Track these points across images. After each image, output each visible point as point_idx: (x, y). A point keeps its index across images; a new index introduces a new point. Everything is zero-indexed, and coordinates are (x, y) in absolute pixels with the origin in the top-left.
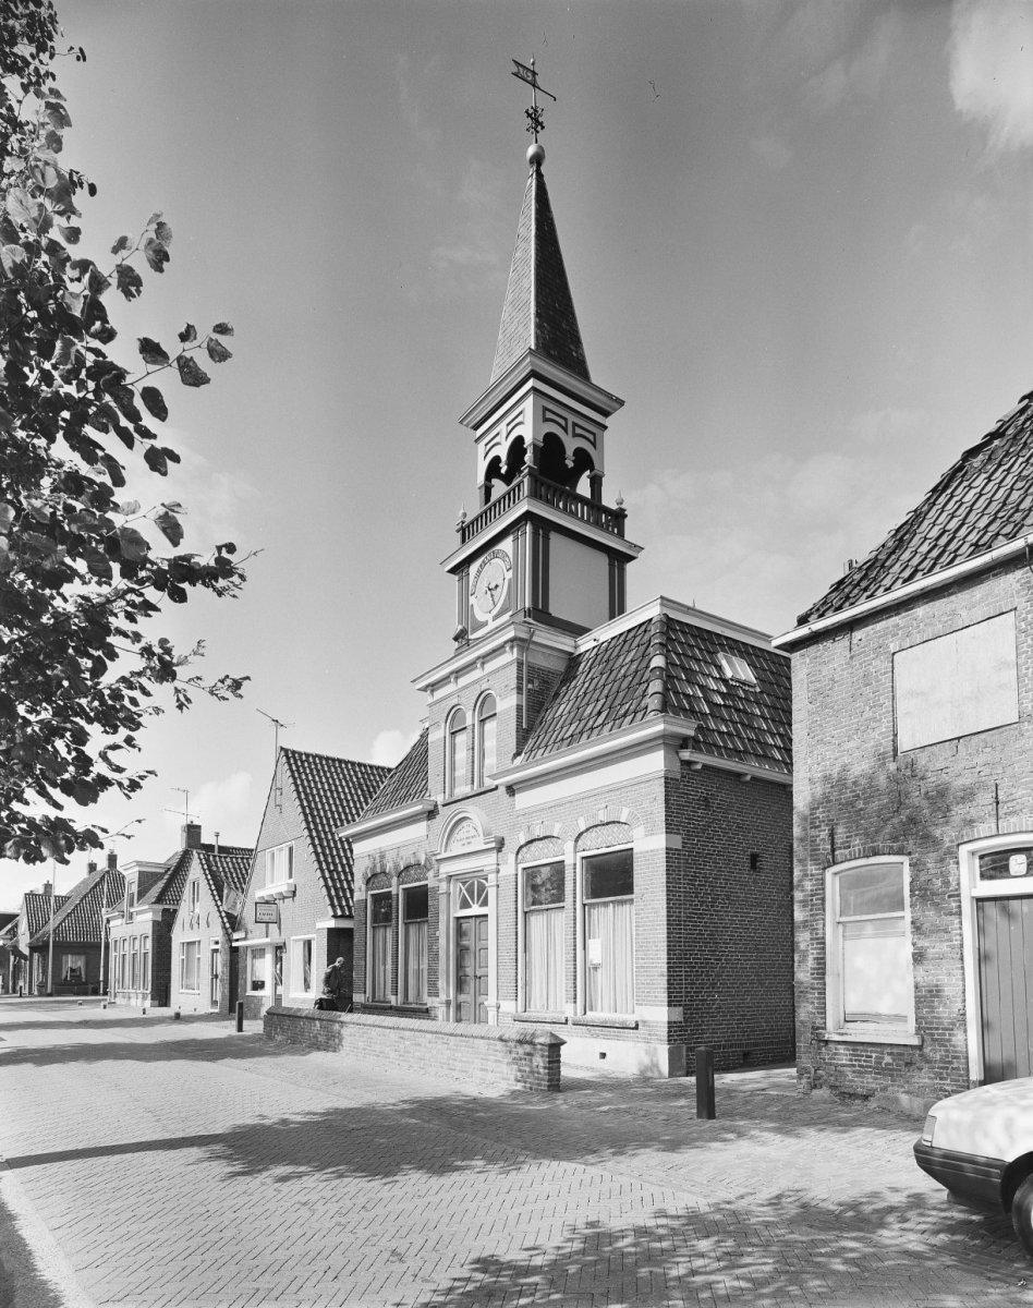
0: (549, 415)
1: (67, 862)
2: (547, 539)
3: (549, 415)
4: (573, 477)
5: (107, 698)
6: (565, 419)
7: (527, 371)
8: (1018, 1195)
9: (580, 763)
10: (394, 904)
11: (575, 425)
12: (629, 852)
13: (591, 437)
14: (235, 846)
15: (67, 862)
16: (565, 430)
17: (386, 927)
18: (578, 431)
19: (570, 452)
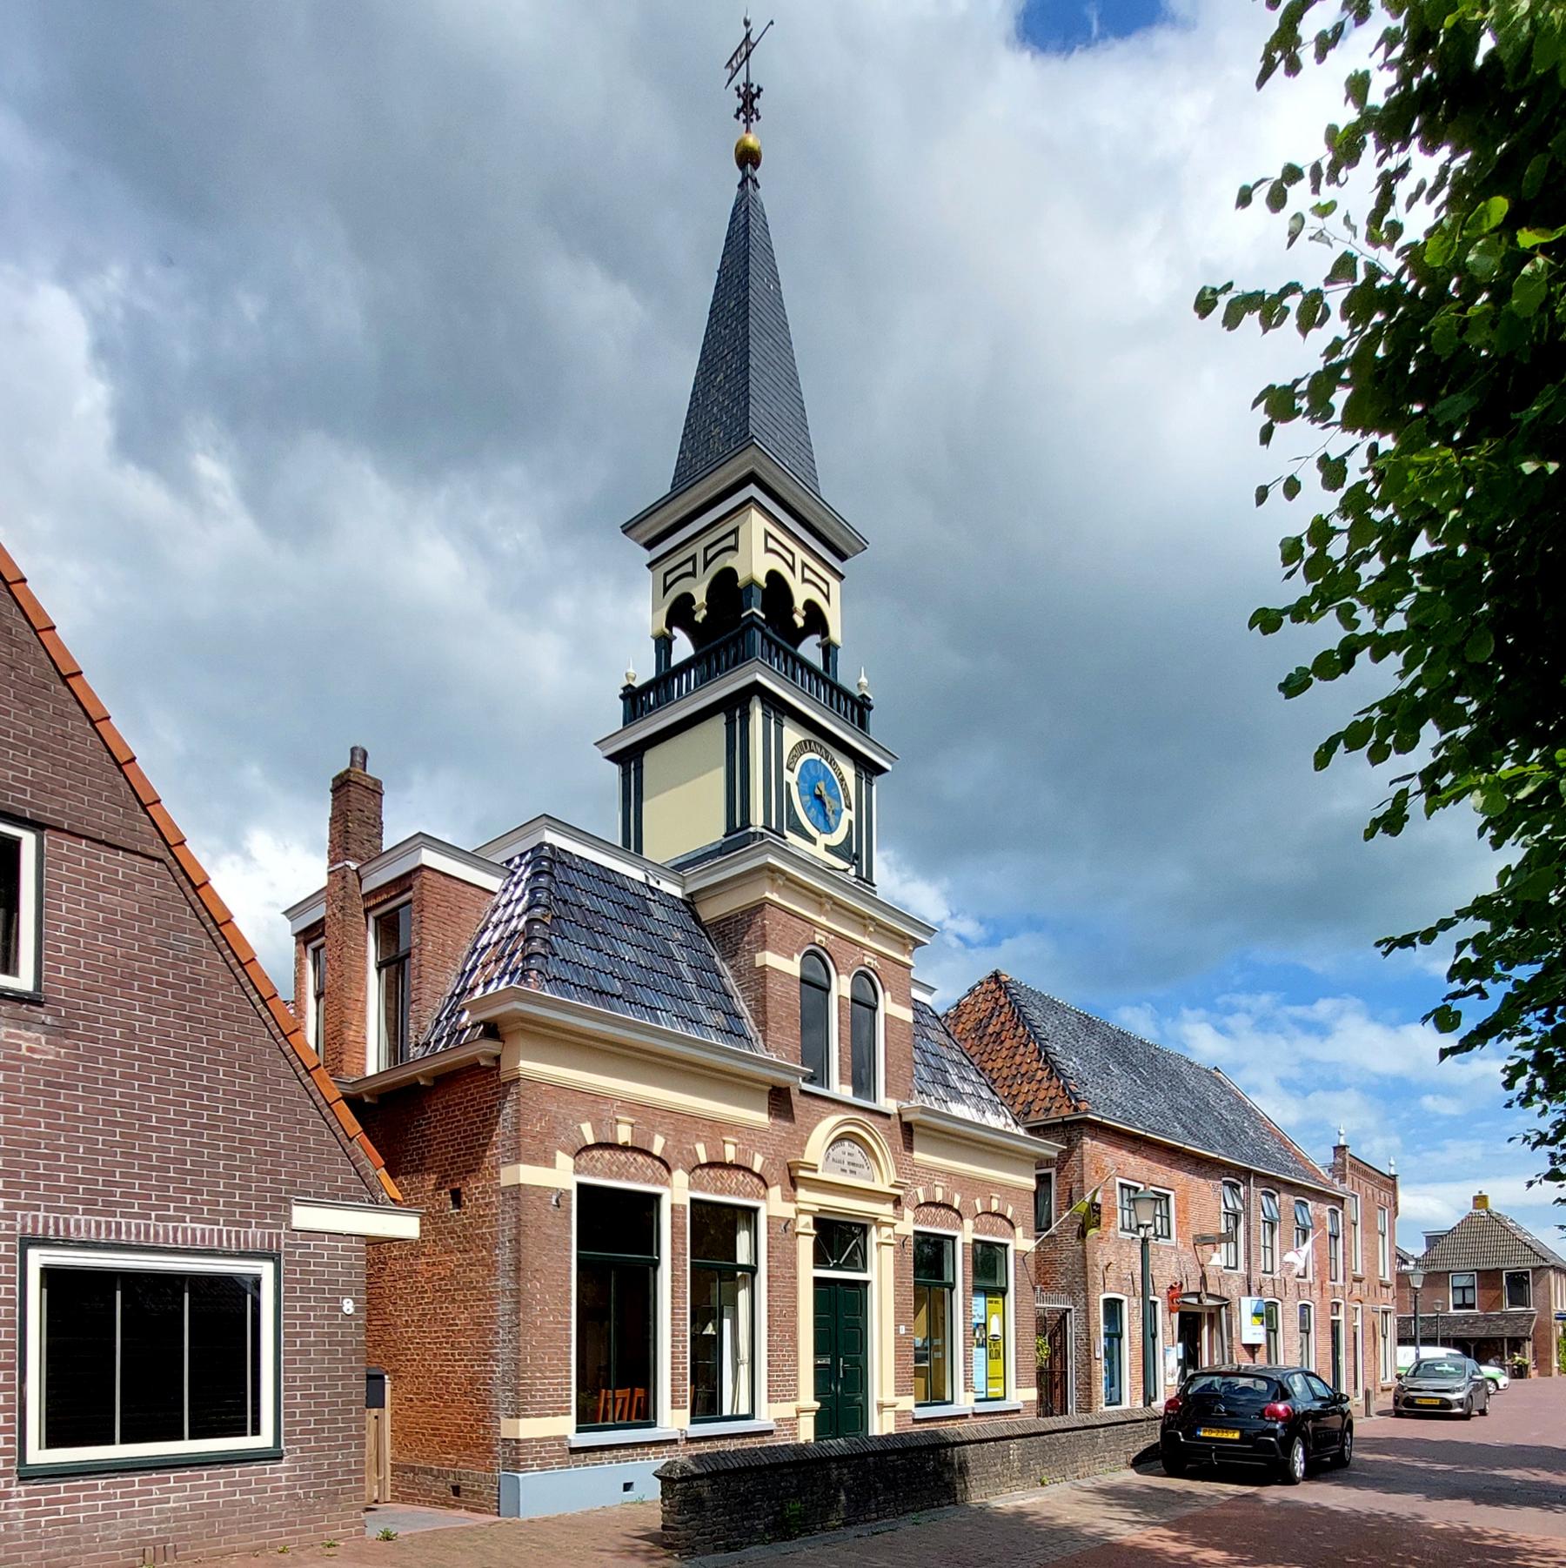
0: (772, 544)
1: (1251, 626)
2: (780, 725)
3: (772, 544)
4: (798, 636)
5: (1452, 733)
6: (792, 554)
7: (745, 471)
8: (1149, 1005)
9: (887, 930)
10: (622, 1023)
11: (804, 565)
12: (860, 1265)
13: (824, 587)
14: (1026, 1390)
15: (1251, 626)
16: (792, 569)
17: (734, 707)
18: (808, 574)
19: (799, 604)
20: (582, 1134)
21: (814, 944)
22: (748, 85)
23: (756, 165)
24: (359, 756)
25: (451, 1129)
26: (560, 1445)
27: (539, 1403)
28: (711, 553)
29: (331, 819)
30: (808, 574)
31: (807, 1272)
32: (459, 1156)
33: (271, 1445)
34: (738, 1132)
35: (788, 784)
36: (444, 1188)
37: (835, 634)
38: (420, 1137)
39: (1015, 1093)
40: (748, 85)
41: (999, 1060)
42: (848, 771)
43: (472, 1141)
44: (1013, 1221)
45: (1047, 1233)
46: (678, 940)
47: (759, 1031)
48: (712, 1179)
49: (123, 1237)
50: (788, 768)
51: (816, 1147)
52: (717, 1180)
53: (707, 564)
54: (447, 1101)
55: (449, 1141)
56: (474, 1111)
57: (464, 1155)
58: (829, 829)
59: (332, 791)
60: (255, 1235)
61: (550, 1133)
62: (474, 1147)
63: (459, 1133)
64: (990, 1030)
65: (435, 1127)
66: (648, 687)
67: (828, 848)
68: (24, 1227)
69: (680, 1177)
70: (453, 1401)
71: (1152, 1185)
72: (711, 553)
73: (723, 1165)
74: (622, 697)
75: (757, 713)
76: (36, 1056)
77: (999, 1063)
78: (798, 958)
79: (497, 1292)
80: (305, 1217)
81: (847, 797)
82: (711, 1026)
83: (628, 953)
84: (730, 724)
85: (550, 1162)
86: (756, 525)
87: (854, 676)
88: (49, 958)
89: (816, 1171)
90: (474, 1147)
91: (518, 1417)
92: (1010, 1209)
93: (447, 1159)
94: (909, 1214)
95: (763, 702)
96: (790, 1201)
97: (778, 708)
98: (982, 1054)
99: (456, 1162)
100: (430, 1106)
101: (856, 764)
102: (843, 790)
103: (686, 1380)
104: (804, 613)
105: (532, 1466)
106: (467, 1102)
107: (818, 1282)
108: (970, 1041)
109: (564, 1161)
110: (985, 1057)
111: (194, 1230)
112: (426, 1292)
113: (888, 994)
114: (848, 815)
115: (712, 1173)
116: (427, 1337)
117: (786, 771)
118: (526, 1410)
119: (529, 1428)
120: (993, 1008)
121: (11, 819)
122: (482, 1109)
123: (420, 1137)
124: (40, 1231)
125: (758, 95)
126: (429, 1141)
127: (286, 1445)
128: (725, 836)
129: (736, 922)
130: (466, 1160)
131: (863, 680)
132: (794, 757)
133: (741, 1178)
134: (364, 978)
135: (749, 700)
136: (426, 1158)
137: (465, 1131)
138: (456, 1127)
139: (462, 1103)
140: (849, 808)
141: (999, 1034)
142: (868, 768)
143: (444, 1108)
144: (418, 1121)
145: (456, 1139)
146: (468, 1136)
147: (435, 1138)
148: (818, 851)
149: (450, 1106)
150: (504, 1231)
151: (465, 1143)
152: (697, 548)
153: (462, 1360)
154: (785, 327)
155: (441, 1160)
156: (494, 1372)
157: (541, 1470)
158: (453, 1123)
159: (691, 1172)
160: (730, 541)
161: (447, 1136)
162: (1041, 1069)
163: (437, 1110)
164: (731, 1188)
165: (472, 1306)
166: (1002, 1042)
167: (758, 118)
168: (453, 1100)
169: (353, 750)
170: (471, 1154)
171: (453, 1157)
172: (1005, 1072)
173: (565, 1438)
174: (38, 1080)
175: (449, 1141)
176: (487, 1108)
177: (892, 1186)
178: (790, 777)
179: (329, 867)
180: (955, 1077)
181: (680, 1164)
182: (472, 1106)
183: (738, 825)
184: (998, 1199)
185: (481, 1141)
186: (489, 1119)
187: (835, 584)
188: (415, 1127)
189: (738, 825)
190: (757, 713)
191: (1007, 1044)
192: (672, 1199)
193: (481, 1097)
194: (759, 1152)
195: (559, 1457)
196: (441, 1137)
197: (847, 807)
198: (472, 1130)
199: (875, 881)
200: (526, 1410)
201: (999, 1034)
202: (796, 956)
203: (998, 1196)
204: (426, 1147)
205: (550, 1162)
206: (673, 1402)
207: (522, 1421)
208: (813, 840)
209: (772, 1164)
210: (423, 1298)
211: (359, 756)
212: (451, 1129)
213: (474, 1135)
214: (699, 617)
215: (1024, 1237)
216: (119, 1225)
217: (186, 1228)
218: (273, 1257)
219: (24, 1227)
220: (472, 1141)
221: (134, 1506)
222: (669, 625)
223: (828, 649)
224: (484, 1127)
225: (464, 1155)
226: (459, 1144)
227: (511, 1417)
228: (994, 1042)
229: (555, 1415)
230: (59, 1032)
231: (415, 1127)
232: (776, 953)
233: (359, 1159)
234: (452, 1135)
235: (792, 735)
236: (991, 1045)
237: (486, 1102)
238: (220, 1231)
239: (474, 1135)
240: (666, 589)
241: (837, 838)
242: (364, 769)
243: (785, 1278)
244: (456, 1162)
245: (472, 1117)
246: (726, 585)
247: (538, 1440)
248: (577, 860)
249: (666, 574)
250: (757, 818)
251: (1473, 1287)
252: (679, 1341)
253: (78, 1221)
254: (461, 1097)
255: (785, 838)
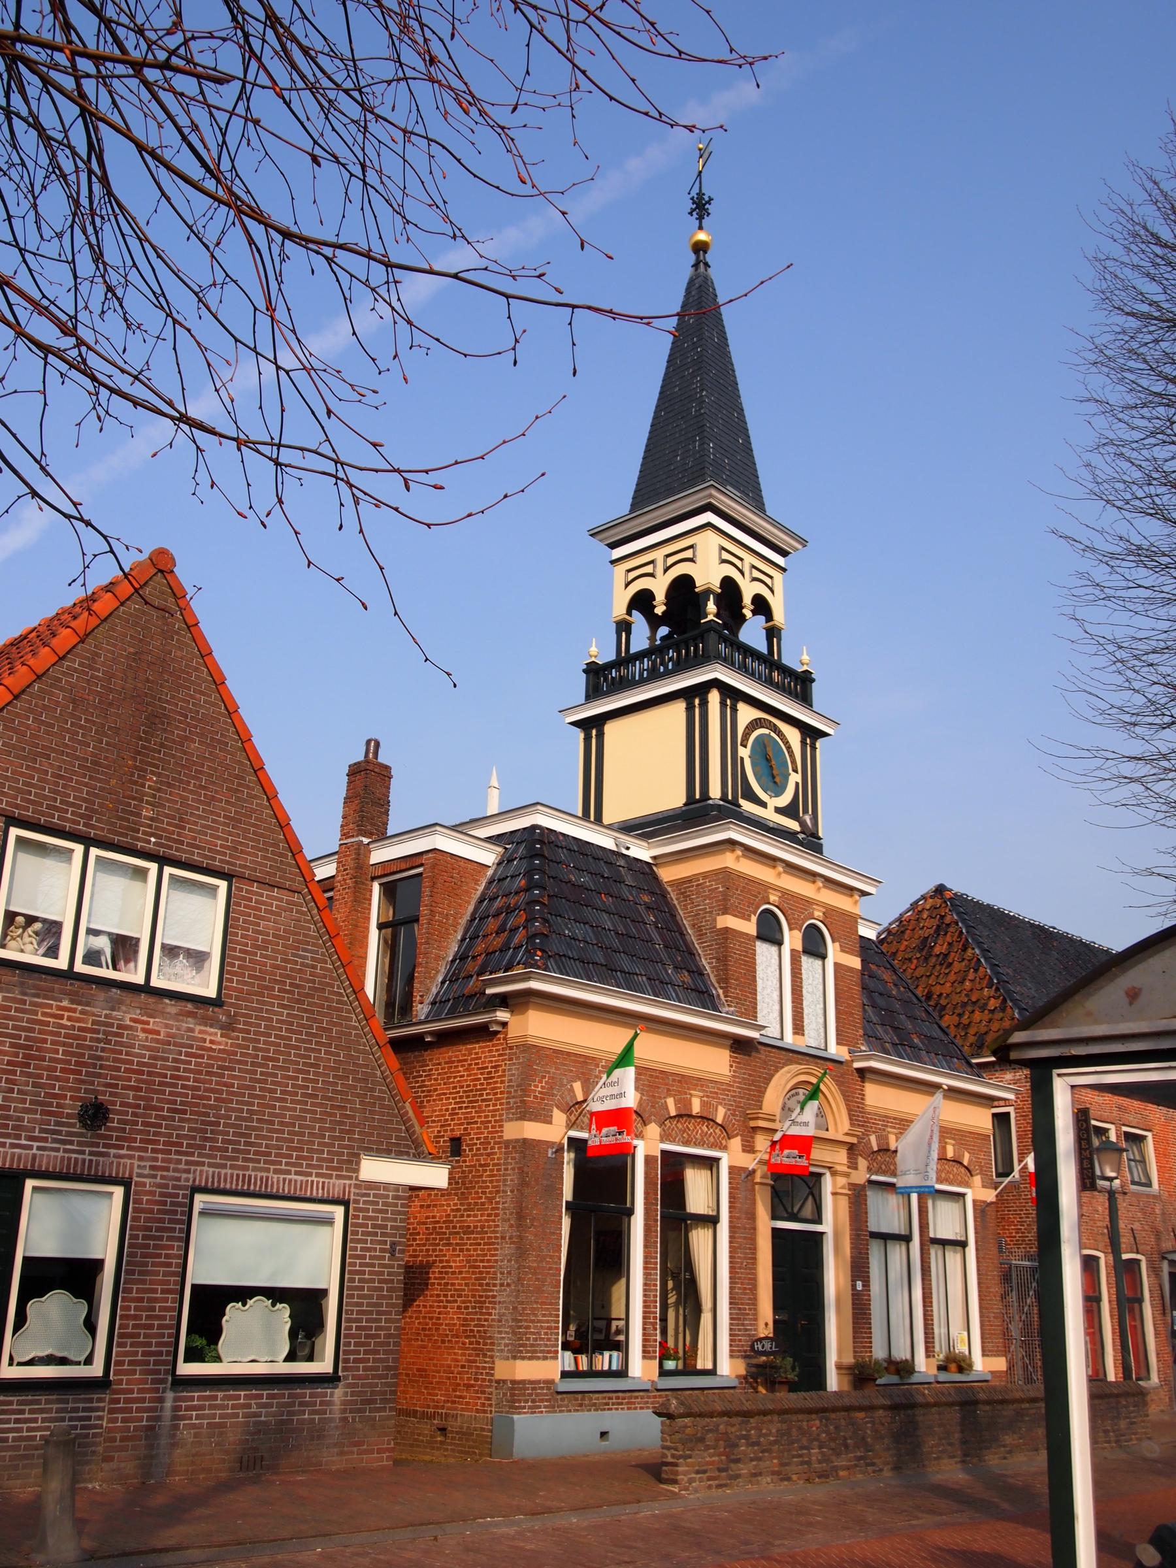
0: (726, 556)
3: (726, 556)
16: (742, 573)
19: (747, 600)
20: (573, 1092)
21: (769, 903)
22: (700, 194)
23: (705, 252)
24: (373, 746)
25: (453, 1082)
26: (549, 1388)
27: (532, 1345)
28: (671, 560)
29: (345, 798)
30: (756, 574)
31: (765, 1225)
32: (460, 1108)
33: (331, 1371)
34: (702, 1086)
35: (742, 759)
36: (443, 1136)
37: (779, 617)
38: (419, 1087)
39: (966, 1022)
40: (700, 194)
41: (948, 985)
42: (793, 736)
43: (474, 1096)
44: (971, 1168)
45: (1009, 1179)
46: (645, 903)
47: (721, 988)
48: (680, 1130)
49: (252, 1187)
50: (742, 745)
51: (773, 1097)
52: (684, 1131)
53: (666, 570)
54: (450, 1057)
55: (450, 1093)
56: (478, 1069)
57: (466, 1108)
58: (778, 790)
59: (348, 775)
60: (337, 1186)
61: (548, 1093)
62: (477, 1101)
63: (462, 1087)
64: (937, 950)
65: (436, 1080)
66: (609, 666)
67: (778, 810)
68: (194, 1180)
69: (653, 1130)
70: (443, 1342)
71: (1124, 1125)
72: (671, 560)
73: (309, 891)
74: (584, 671)
75: (714, 697)
76: (214, 1047)
77: (947, 988)
78: (754, 919)
79: (496, 1238)
80: (375, 1169)
81: (794, 762)
82: (679, 986)
83: (607, 922)
84: (690, 709)
85: (548, 1120)
86: (709, 543)
87: (796, 656)
88: (229, 972)
89: (774, 1121)
90: (477, 1101)
91: (515, 1358)
92: (967, 1155)
93: (447, 1110)
94: (862, 1163)
95: (721, 693)
96: (749, 1152)
97: (732, 695)
98: (928, 977)
99: (458, 1114)
100: (431, 1060)
101: (802, 733)
102: (790, 756)
103: (656, 1329)
104: (752, 607)
105: (524, 1407)
106: (472, 1060)
107: (776, 1232)
108: (915, 961)
109: (559, 1117)
110: (932, 981)
111: (296, 1181)
112: (418, 1234)
113: (837, 944)
114: (795, 778)
115: (679, 1125)
116: (417, 1278)
117: (740, 749)
118: (521, 1352)
119: (527, 1370)
120: (938, 926)
121: (1094, 1351)
122: (487, 1067)
123: (419, 1087)
124: (210, 1184)
125: (709, 202)
126: (429, 1091)
127: (343, 1371)
128: (685, 805)
129: (697, 885)
130: (467, 1113)
131: (805, 658)
132: (746, 735)
133: (705, 1129)
134: (366, 937)
135: (708, 692)
136: (425, 1107)
137: (468, 1086)
138: (459, 1081)
139: (466, 1060)
140: (796, 771)
141: (946, 956)
142: (811, 734)
143: (446, 1063)
144: (419, 1071)
145: (459, 1092)
146: (471, 1091)
147: (436, 1090)
148: (769, 815)
149: (453, 1062)
150: (505, 1180)
151: (468, 1097)
152: (658, 555)
153: (456, 1301)
154: (741, 423)
155: (441, 1110)
156: (490, 1314)
157: (532, 1413)
158: (455, 1077)
159: (662, 1124)
160: (688, 554)
161: (448, 1089)
162: (994, 997)
163: (439, 1064)
164: (696, 1139)
165: (468, 1250)
166: (950, 964)
167: (709, 214)
168: (456, 1056)
169: (368, 742)
170: (473, 1107)
171: (454, 1109)
172: (956, 999)
173: (552, 1382)
174: (213, 1065)
175: (450, 1093)
176: (492, 1067)
177: (847, 1134)
178: (744, 752)
179: (340, 840)
180: (902, 1017)
181: (653, 1117)
182: (477, 1064)
183: (698, 797)
184: (953, 1145)
185: (485, 1097)
186: (493, 1077)
187: (777, 575)
188: (414, 1077)
189: (698, 797)
190: (714, 697)
191: (957, 966)
192: (8, 902)
193: (485, 1057)
194: (721, 1104)
195: (547, 1401)
196: (442, 1089)
197: (794, 771)
198: (475, 1085)
199: (820, 834)
200: (521, 1352)
201: (946, 956)
202: (753, 916)
203: (953, 1142)
204: (426, 1096)
205: (548, 1120)
206: (644, 1352)
207: (519, 1362)
208: (763, 805)
209: (734, 1115)
210: (415, 1240)
211: (373, 746)
212: (453, 1082)
213: (477, 1090)
214: (660, 610)
215: (984, 1187)
216: (250, 1176)
217: (290, 1181)
218: (345, 1203)
219: (194, 1180)
220: (474, 1096)
221: (238, 1417)
222: (629, 613)
223: (773, 633)
224: (488, 1084)
225: (466, 1108)
226: (461, 1097)
227: (507, 1358)
228: (941, 964)
229: (545, 1358)
230: (228, 1028)
231: (414, 1077)
232: (735, 916)
233: (409, 1119)
234: (455, 1088)
235: (746, 714)
236: (938, 967)
237: (491, 1062)
238: (312, 1182)
239: (477, 1090)
240: (627, 585)
241: (785, 800)
242: (377, 758)
243: (745, 1229)
244: (458, 1114)
245: (476, 1074)
246: (683, 587)
247: (531, 1382)
248: (561, 838)
249: (629, 571)
250: (715, 792)
251: (963, 1244)
252: (650, 1291)
253: (226, 1174)
254: (465, 1055)
255: (740, 806)
